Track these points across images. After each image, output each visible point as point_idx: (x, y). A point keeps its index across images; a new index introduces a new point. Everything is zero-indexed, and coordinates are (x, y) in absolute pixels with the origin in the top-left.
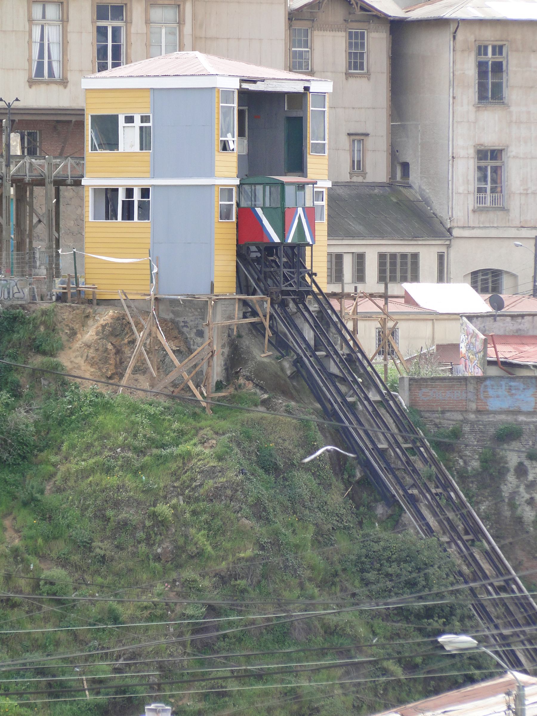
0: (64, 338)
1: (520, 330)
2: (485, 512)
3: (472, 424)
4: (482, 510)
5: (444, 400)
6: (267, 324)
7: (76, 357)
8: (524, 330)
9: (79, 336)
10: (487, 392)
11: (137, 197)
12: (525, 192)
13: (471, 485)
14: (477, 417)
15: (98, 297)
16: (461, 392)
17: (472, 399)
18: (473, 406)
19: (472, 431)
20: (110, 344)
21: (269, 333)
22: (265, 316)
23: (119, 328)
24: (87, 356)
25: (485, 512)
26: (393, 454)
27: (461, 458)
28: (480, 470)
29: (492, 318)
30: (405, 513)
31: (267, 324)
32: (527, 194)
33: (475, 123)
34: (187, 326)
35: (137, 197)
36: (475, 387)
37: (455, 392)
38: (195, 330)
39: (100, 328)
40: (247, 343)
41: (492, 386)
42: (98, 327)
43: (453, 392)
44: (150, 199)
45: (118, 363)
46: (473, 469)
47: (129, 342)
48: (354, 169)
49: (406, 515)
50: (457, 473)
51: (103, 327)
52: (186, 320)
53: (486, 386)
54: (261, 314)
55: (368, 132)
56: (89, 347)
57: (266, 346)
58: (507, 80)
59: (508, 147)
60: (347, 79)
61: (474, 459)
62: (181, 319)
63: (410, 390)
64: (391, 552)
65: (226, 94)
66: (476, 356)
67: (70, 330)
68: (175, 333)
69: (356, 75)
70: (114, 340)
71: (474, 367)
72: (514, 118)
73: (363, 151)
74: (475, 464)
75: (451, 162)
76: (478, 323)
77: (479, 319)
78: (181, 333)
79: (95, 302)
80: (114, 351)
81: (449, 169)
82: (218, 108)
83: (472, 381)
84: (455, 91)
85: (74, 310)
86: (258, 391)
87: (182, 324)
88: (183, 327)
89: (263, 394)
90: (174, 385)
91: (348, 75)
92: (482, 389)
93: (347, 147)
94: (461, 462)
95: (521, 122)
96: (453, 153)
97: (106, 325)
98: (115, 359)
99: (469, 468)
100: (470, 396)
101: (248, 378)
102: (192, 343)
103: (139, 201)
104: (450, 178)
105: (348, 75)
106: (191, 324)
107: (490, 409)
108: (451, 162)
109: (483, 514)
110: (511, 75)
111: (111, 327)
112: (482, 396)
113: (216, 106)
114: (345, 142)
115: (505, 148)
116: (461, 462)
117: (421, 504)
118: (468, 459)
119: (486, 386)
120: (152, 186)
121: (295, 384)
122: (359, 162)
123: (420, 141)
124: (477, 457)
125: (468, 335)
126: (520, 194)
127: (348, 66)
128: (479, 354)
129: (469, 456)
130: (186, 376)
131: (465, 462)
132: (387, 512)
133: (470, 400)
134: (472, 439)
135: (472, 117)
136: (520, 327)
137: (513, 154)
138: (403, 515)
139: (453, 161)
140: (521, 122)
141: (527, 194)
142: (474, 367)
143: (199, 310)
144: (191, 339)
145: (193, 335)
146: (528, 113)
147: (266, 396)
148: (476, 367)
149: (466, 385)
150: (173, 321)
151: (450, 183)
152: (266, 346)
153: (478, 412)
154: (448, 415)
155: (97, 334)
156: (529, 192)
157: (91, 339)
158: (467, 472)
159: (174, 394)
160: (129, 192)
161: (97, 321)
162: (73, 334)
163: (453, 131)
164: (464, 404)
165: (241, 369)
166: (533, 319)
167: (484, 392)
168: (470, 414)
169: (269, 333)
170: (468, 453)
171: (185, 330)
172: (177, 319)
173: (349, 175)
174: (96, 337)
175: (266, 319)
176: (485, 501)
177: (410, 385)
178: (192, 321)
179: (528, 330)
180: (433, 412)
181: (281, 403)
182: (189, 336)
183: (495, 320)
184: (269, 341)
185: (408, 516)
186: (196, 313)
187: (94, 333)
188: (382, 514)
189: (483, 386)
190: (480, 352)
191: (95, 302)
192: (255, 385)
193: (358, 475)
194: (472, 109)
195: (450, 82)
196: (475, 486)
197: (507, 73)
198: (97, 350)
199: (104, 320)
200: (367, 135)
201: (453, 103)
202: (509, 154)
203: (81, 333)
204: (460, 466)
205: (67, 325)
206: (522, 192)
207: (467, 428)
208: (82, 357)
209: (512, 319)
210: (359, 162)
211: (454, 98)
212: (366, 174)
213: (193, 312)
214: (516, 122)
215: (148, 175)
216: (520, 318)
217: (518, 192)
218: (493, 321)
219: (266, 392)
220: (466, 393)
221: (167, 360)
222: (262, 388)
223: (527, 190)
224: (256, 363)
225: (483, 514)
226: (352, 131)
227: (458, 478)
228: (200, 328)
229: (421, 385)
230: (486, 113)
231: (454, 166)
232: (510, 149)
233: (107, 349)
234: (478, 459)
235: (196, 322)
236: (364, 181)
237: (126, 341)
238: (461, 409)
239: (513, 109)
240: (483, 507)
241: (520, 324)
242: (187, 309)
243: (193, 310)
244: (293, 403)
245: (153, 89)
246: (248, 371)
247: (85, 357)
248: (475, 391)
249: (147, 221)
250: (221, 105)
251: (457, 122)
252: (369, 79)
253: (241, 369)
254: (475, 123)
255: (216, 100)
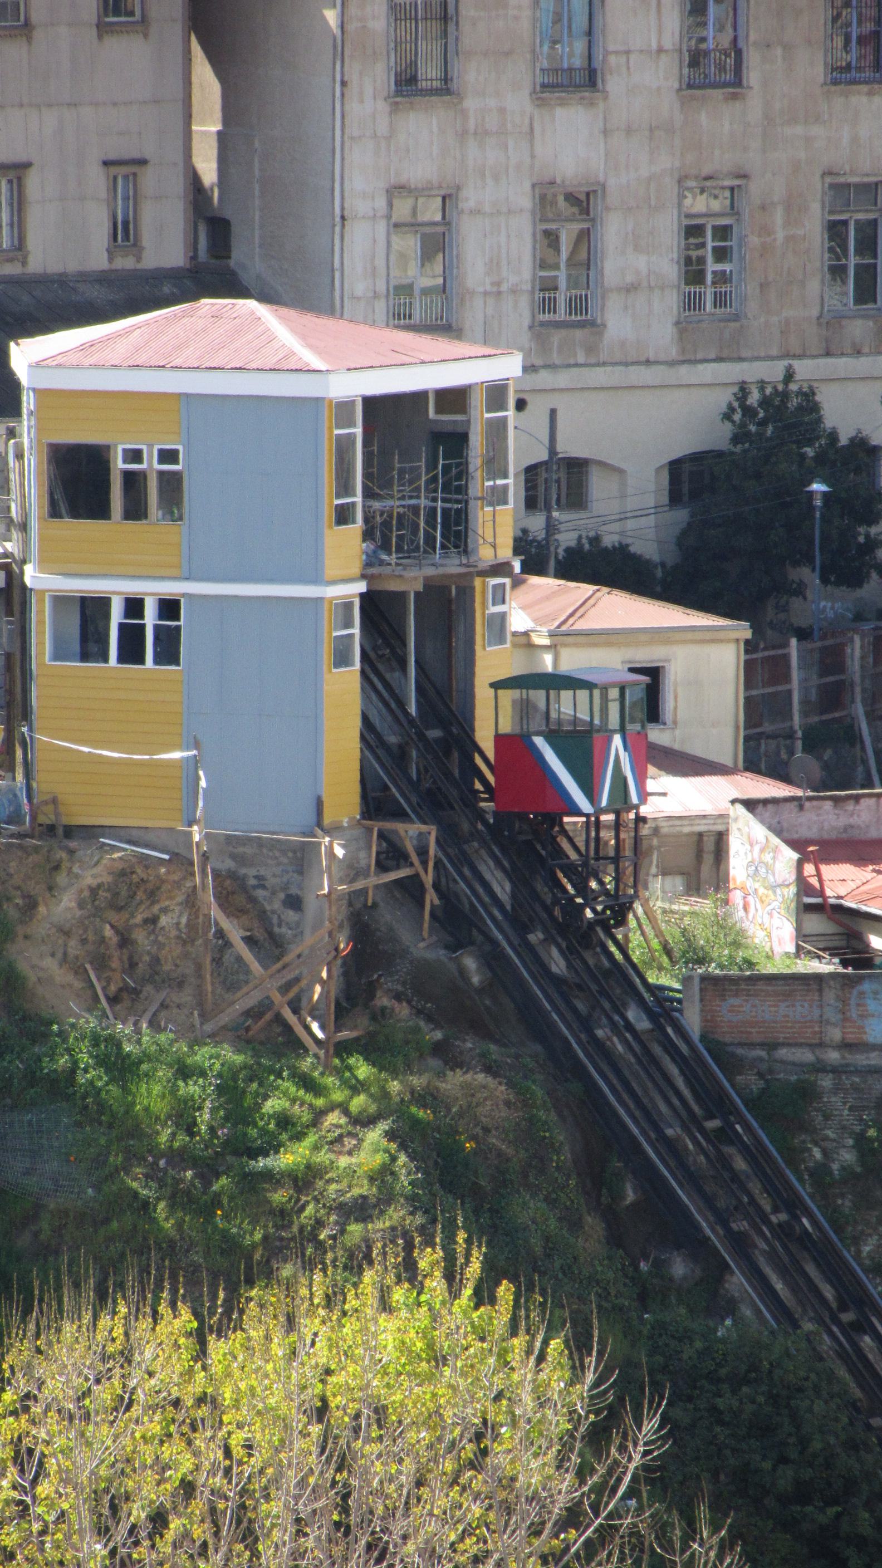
0: (13, 913)
1: (852, 827)
2: (872, 1259)
3: (836, 1070)
4: (864, 1254)
5: (775, 1022)
6: (428, 879)
7: (41, 956)
8: (859, 827)
9: (42, 909)
10: (864, 1005)
11: (150, 618)
12: (495, 289)
13: (840, 1202)
14: (843, 1058)
15: (66, 821)
16: (811, 1006)
17: (833, 1020)
18: (835, 1034)
19: (837, 1089)
20: (108, 927)
21: (431, 897)
22: (424, 863)
23: (124, 893)
24: (65, 954)
25: (872, 1259)
26: (691, 1147)
27: (816, 1144)
28: (859, 1170)
29: (796, 803)
30: (732, 1273)
31: (428, 879)
32: (499, 293)
33: (388, 139)
34: (264, 887)
35: (150, 618)
36: (838, 996)
37: (797, 1004)
38: (282, 896)
39: (86, 893)
40: (388, 917)
41: (876, 993)
42: (81, 891)
43: (793, 1006)
44: (181, 623)
45: (127, 966)
46: (843, 1168)
47: (146, 921)
48: (115, 239)
49: (734, 1279)
50: (811, 1175)
51: (94, 891)
52: (262, 873)
53: (862, 993)
54: (415, 858)
55: (148, 157)
56: (67, 934)
57: (426, 925)
58: (457, 39)
59: (458, 188)
60: (100, 37)
61: (844, 1147)
62: (252, 872)
63: (701, 1000)
64: (713, 1359)
65: (343, 409)
66: (775, 892)
67: (24, 897)
68: (240, 900)
69: (117, 28)
70: (112, 916)
71: (771, 915)
72: (471, 124)
73: (134, 199)
74: (848, 1157)
75: (337, 229)
76: (767, 814)
77: (770, 806)
78: (253, 900)
79: (60, 831)
80: (115, 940)
81: (333, 246)
82: (330, 439)
83: (832, 983)
84: (346, 69)
85: (29, 854)
86: (422, 1024)
87: (252, 882)
88: (255, 887)
89: (433, 1030)
90: (254, 1013)
91: (103, 29)
92: (853, 1002)
93: (103, 193)
94: (817, 1153)
95: (486, 133)
96: (343, 209)
97: (99, 886)
98: (120, 959)
99: (835, 1167)
100: (830, 1014)
101: (398, 997)
102: (275, 921)
103: (156, 628)
104: (337, 264)
105: (103, 29)
106: (271, 881)
107: (871, 1040)
108: (337, 229)
109: (867, 1262)
110: (465, 26)
111: (108, 890)
112: (854, 1013)
113: (326, 436)
114: (97, 179)
115: (453, 191)
116: (817, 1153)
117: (757, 1252)
118: (828, 1145)
119: (862, 993)
120: (183, 595)
121: (487, 1002)
122: (126, 224)
123: (257, 173)
124: (850, 1142)
125: (751, 845)
126: (486, 293)
127: (101, 10)
128: (786, 890)
129: (834, 1140)
130: (277, 998)
131: (825, 1152)
132: (693, 1271)
133: (828, 1022)
134: (839, 1105)
135: (382, 127)
136: (852, 821)
137: (471, 204)
138: (727, 1277)
139: (343, 226)
140: (486, 133)
141: (499, 293)
142: (771, 915)
143: (290, 854)
144: (273, 912)
145: (277, 905)
146: (502, 111)
147: (438, 1035)
148: (776, 915)
149: (820, 990)
150: (232, 875)
151: (337, 274)
152: (426, 925)
153: (846, 1046)
154: (783, 1053)
155: (81, 905)
156: (504, 287)
157: (69, 916)
158: (831, 1173)
159: (251, 1033)
160: (134, 606)
161: (77, 876)
162: (295, 903)
163: (343, 159)
164: (817, 1029)
165: (380, 976)
166: (878, 804)
167: (858, 1005)
168: (830, 1050)
169: (431, 897)
170: (829, 1133)
171: (260, 893)
172: (243, 871)
173: (105, 255)
174: (78, 913)
175: (426, 872)
176: (870, 1235)
177: (701, 990)
178: (274, 876)
179: (868, 826)
180: (752, 1045)
181: (471, 1049)
182: (268, 908)
183: (801, 807)
184: (432, 914)
185: (737, 1282)
186: (285, 861)
187: (73, 904)
188: (685, 1278)
189: (855, 992)
190: (788, 886)
191: (60, 831)
192: (414, 1011)
193: (630, 1196)
194: (382, 106)
195: (335, 47)
196: (848, 1203)
197: (457, 24)
198: (84, 941)
199: (94, 876)
200: (142, 162)
201: (343, 95)
202: (460, 205)
203: (46, 905)
204: (816, 1162)
205: (18, 888)
206: (488, 288)
207: (826, 1082)
208: (53, 955)
209: (835, 806)
210: (126, 224)
211: (344, 83)
212: (141, 249)
213: (276, 858)
214: (475, 133)
215: (175, 572)
216: (852, 802)
217: (481, 289)
218: (796, 810)
219: (438, 1026)
220: (821, 1006)
221: (228, 958)
222: (429, 1019)
223: (498, 284)
224: (411, 962)
225: (867, 1262)
226: (112, 156)
227: (811, 1185)
228: (294, 891)
229: (724, 990)
230: (412, 115)
231: (346, 239)
232: (463, 194)
233: (104, 937)
234: (853, 1147)
235: (285, 879)
236: (139, 266)
237: (139, 919)
238: (809, 1041)
239: (471, 103)
240: (868, 1249)
241: (852, 815)
242: (265, 851)
243: (277, 854)
244: (493, 1047)
245: (187, 396)
246: (398, 980)
247: (59, 955)
248: (840, 1005)
249: (173, 667)
250: (337, 432)
251: (352, 138)
252: (146, 36)
253: (380, 976)
254: (388, 139)
255: (326, 424)
